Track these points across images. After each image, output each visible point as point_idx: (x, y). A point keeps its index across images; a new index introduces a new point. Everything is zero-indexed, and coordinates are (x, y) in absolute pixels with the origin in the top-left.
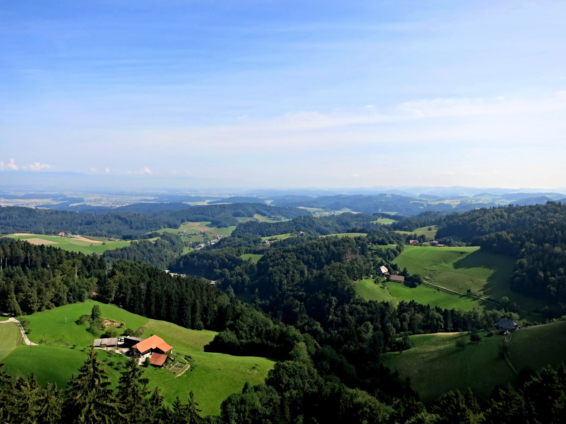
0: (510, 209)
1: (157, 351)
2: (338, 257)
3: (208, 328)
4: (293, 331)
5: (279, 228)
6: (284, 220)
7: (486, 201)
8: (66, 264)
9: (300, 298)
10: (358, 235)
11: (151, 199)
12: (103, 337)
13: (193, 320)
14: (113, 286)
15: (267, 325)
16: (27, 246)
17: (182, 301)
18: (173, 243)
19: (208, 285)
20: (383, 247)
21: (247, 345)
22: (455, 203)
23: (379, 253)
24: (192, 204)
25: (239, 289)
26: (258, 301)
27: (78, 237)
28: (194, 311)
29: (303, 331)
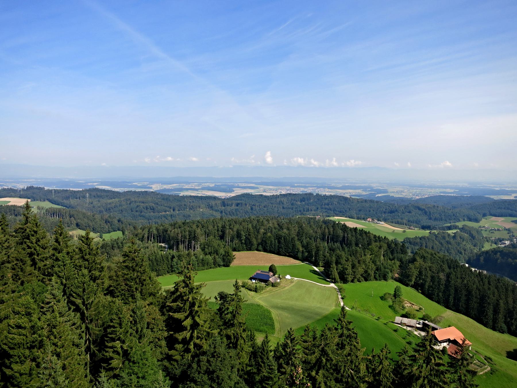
11: (450, 192)
12: (403, 316)
13: (495, 321)
16: (345, 228)
18: (473, 237)
24: (495, 197)
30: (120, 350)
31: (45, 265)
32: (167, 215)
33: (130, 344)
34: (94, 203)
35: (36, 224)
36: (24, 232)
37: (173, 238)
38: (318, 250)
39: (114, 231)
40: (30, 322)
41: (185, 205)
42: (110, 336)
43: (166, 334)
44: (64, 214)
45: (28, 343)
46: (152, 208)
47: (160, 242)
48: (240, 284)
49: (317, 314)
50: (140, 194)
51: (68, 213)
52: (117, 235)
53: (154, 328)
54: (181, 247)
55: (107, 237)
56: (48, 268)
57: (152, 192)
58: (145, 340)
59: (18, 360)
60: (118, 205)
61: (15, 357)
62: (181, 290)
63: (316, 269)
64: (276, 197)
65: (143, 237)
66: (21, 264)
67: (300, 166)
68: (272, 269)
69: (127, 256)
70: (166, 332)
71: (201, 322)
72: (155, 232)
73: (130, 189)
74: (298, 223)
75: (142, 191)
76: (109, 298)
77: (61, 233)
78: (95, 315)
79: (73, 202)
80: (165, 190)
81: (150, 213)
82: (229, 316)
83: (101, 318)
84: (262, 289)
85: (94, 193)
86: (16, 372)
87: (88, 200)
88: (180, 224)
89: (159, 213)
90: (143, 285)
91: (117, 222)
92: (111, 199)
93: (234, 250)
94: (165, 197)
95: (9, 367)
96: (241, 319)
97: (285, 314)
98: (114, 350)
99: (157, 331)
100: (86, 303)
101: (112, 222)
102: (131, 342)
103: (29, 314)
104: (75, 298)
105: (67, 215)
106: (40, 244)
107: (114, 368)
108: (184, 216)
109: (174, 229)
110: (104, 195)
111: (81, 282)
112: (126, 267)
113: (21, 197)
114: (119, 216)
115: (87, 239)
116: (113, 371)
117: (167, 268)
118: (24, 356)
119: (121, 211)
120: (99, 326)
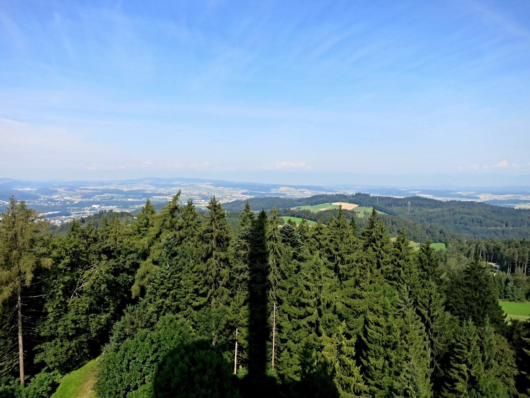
30: (466, 374)
31: (387, 269)
32: (498, 230)
33: (478, 371)
34: (415, 212)
35: (382, 229)
36: (369, 236)
37: (507, 259)
39: (435, 242)
40: (387, 322)
41: (522, 220)
42: (457, 356)
43: (516, 372)
44: (387, 221)
45: (383, 341)
46: (479, 221)
47: (490, 261)
50: (465, 205)
51: (391, 220)
53: (501, 361)
56: (390, 272)
57: (480, 203)
58: (491, 371)
59: (374, 354)
60: (440, 215)
61: (371, 351)
65: (469, 252)
66: (371, 265)
69: (469, 273)
70: (517, 370)
72: (484, 249)
73: (454, 199)
75: (467, 201)
77: (404, 240)
78: (440, 329)
79: (395, 209)
80: (495, 201)
81: (476, 226)
83: (445, 334)
85: (416, 202)
86: (371, 365)
87: (409, 208)
88: (517, 242)
89: (487, 227)
90: (486, 308)
91: (438, 233)
92: (433, 208)
94: (496, 210)
95: (366, 358)
98: (460, 373)
99: (505, 366)
100: (432, 315)
101: (433, 232)
102: (478, 369)
103: (386, 314)
104: (421, 307)
105: (390, 222)
106: (384, 249)
107: (459, 392)
108: (520, 233)
109: (509, 248)
110: (426, 204)
111: (428, 292)
112: (468, 284)
113: (350, 202)
114: (441, 227)
115: (428, 248)
116: (456, 394)
117: (499, 292)
118: (379, 352)
119: (443, 222)
120: (443, 343)
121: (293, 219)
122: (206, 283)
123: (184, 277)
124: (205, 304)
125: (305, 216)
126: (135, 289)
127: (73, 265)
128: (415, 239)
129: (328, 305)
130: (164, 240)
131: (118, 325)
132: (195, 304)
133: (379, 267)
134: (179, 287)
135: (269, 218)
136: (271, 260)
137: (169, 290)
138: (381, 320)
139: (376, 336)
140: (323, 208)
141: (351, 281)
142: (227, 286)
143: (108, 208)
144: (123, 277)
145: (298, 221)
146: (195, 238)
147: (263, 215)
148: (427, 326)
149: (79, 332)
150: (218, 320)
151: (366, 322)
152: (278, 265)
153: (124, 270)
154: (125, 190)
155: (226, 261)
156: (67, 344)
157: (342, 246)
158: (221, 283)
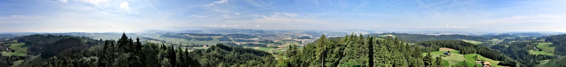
0: (558, 36)
1: (488, 65)
2: (525, 46)
3: (498, 60)
4: (516, 61)
5: (513, 40)
6: (514, 38)
7: (554, 34)
8: (471, 46)
9: (517, 54)
10: (529, 41)
11: (487, 34)
12: (478, 61)
13: (495, 59)
14: (480, 51)
15: (510, 60)
16: (465, 42)
17: (493, 55)
18: (491, 43)
19: (498, 52)
20: (535, 43)
21: (507, 64)
22: (548, 34)
23: (534, 45)
24: (495, 35)
25: (504, 52)
26: (509, 55)
27: (473, 41)
28: (495, 57)
29: (518, 61)
38: (459, 47)
48: (441, 55)
49: (459, 62)
52: (414, 44)
54: (428, 47)
55: (412, 44)
62: (428, 56)
63: (459, 51)
64: (449, 35)
67: (455, 28)
68: (448, 52)
71: (432, 64)
74: (454, 41)
76: (412, 57)
82: (439, 62)
84: (446, 56)
93: (440, 47)
96: (441, 63)
97: (451, 62)
103: (399, 58)
113: (391, 34)
121: (379, 38)
122: (359, 52)
123: (354, 51)
124: (359, 57)
125: (381, 37)
126: (344, 54)
127: (332, 48)
128: (405, 42)
129: (387, 57)
130: (350, 43)
131: (341, 61)
132: (357, 57)
133: (398, 48)
134: (353, 53)
135: (373, 38)
136: (374, 47)
137: (351, 54)
138: (398, 60)
139: (397, 63)
140: (385, 36)
141: (392, 52)
142: (364, 53)
143: (339, 36)
144: (342, 51)
145: (380, 39)
146: (357, 43)
147: (372, 37)
148: (408, 60)
149: (333, 61)
150: (362, 61)
151: (395, 60)
152: (375, 48)
153: (342, 49)
154: (342, 32)
155: (364, 48)
156: (331, 63)
157: (390, 44)
158: (363, 52)
